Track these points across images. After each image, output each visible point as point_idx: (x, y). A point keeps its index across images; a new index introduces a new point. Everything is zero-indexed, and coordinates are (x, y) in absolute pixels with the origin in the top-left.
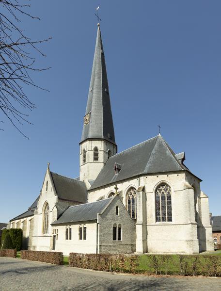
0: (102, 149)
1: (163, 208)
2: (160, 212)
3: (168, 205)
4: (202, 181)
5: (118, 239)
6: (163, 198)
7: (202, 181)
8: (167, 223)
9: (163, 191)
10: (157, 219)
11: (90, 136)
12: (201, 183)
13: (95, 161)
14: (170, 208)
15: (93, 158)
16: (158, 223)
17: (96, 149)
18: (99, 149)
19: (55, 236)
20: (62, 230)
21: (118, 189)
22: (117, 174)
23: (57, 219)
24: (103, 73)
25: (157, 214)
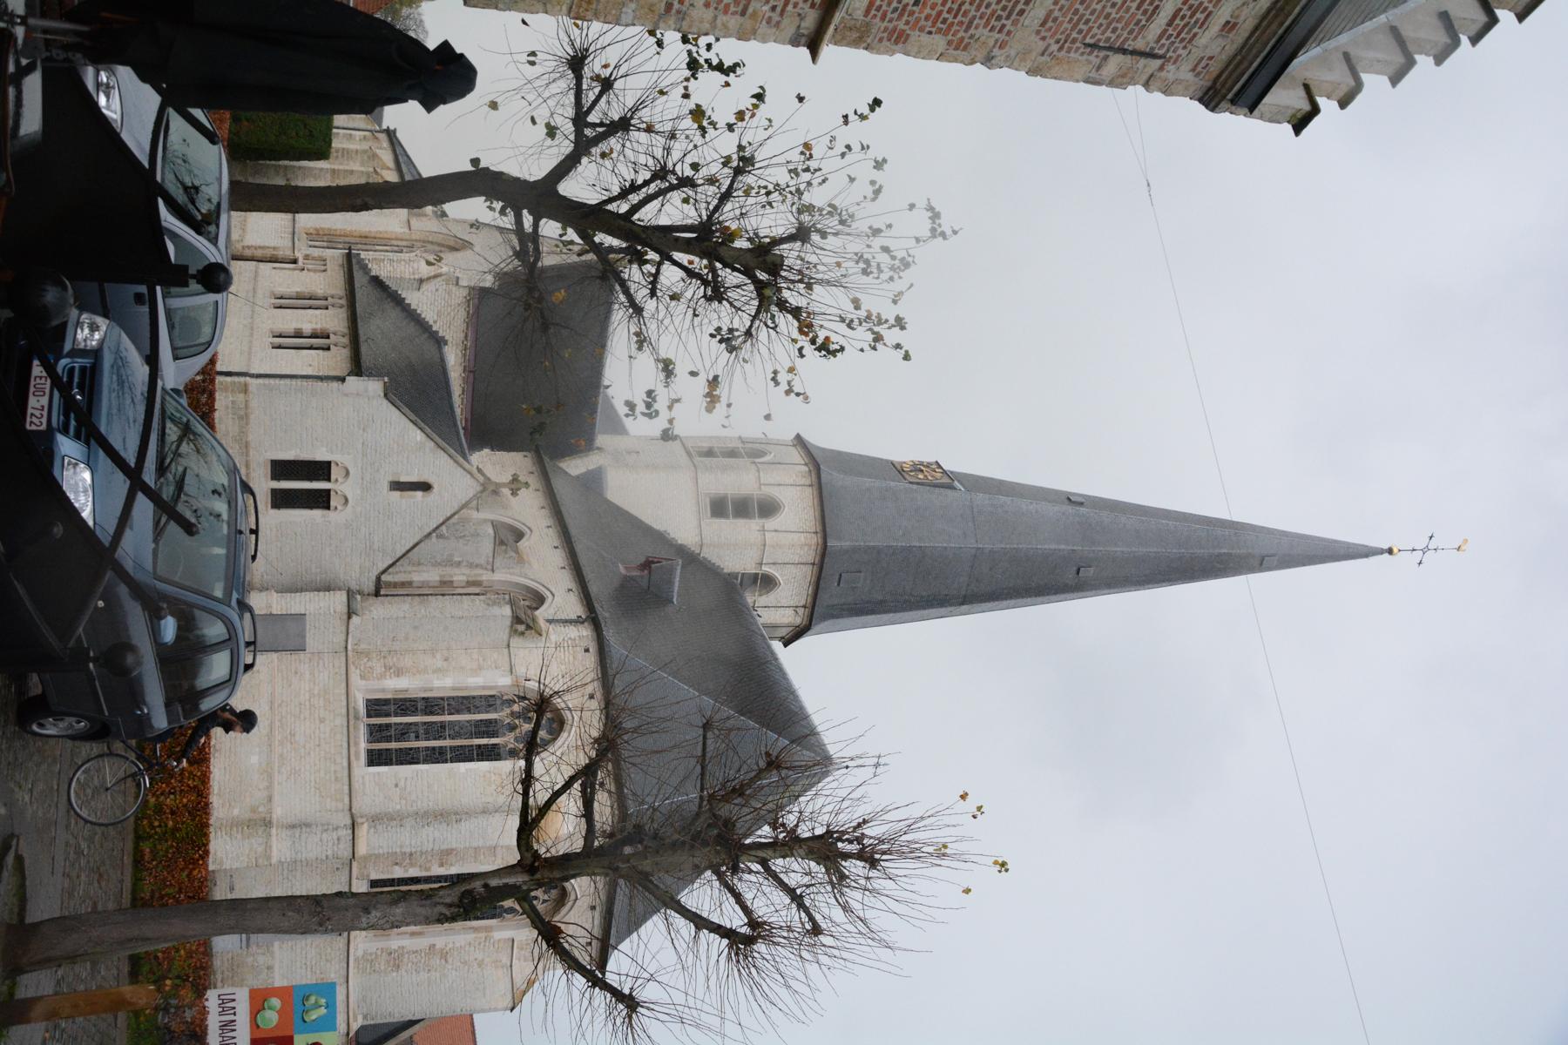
1: (438, 731)
3: (453, 749)
4: (814, 54)
5: (274, 492)
6: (489, 728)
7: (814, 54)
8: (363, 745)
10: (376, 707)
14: (437, 756)
17: (768, 508)
18: (771, 523)
19: (295, 261)
20: (328, 282)
21: (514, 493)
25: (406, 705)
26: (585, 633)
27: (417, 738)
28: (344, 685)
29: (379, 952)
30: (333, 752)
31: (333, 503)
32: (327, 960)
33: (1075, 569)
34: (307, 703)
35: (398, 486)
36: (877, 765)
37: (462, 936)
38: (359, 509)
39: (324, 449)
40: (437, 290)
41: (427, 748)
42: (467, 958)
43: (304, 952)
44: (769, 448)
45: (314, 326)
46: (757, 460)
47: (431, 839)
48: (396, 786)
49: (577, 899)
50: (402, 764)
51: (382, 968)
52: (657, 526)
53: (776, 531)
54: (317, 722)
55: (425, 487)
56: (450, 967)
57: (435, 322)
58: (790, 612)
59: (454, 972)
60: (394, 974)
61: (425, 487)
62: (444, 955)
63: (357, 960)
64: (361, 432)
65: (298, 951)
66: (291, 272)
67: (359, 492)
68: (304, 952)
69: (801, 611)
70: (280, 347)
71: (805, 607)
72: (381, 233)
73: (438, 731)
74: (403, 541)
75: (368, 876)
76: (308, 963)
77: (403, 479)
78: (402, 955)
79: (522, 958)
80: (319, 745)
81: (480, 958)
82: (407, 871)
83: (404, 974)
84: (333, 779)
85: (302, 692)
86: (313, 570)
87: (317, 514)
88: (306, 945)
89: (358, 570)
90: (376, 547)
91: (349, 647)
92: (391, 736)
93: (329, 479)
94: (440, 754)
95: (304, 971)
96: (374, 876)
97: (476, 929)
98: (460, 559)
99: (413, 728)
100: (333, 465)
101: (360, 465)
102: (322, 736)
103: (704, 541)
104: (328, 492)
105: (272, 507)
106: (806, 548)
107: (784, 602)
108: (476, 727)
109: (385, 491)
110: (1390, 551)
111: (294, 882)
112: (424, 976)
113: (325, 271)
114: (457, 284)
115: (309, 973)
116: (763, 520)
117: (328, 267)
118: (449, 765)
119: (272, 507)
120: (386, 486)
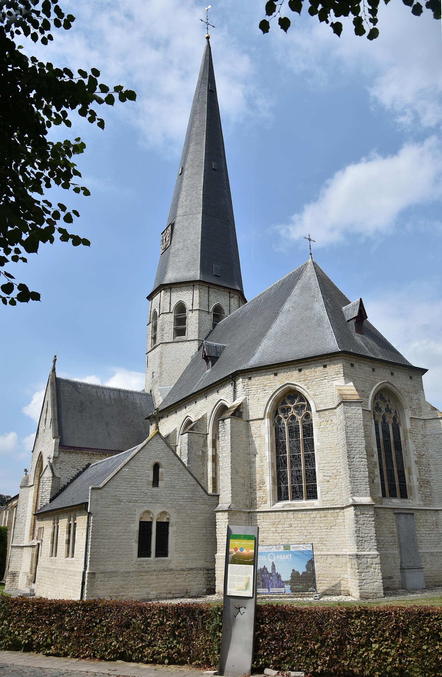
0: (196, 307)
1: (295, 459)
2: (285, 473)
3: (305, 450)
5: (157, 555)
6: (293, 431)
9: (293, 412)
11: (170, 278)
12: (425, 377)
13: (178, 338)
15: (172, 331)
16: (280, 505)
18: (189, 306)
22: (209, 370)
23: (51, 500)
24: (209, 119)
26: (241, 380)
27: (300, 471)
28: (270, 514)
29: (421, 492)
30: (309, 519)
31: (165, 520)
32: (426, 522)
33: (213, 171)
34: (280, 534)
35: (155, 483)
36: (310, 240)
37: (410, 446)
38: (168, 505)
39: (132, 525)
40: (60, 468)
41: (306, 465)
42: (422, 444)
43: (423, 535)
44: (153, 309)
45: (65, 533)
46: (158, 315)
47: (360, 460)
48: (328, 481)
49: (387, 382)
50: (315, 479)
51: (429, 490)
52: (189, 361)
53: (193, 305)
54: (292, 528)
55: (156, 467)
56: (426, 453)
57: (78, 469)
58: (232, 300)
59: (429, 451)
60: (432, 484)
61: (156, 467)
62: (420, 456)
63: (425, 505)
64: (122, 503)
65: (422, 538)
66: (43, 547)
67: (158, 505)
68: (423, 535)
69: (232, 295)
70: (73, 552)
71: (230, 293)
72: (34, 500)
73: (295, 459)
74: (188, 480)
75: (380, 498)
76: (428, 532)
77: (151, 479)
78: (421, 479)
79: (420, 414)
80: (305, 527)
81: (421, 436)
82: (377, 475)
83: (431, 479)
84: (325, 518)
85: (274, 537)
86: (204, 531)
87: (171, 530)
88: (419, 534)
89: (205, 506)
90: (191, 496)
91: (248, 510)
92: (299, 486)
93: (151, 523)
94: (309, 457)
95: (432, 535)
96: (380, 495)
97: (406, 438)
98: (201, 451)
99: (294, 473)
100: (143, 520)
101: (142, 504)
102: (300, 525)
103: (197, 338)
104: (157, 523)
105: (166, 556)
106: (201, 290)
107: (227, 302)
108: (293, 438)
109: (160, 490)
110: (208, 38)
111: (385, 541)
112: (432, 467)
113: (43, 527)
114: (57, 458)
115: (434, 532)
116: (187, 310)
117: (42, 526)
118: (315, 452)
119: (166, 556)
120: (155, 489)
